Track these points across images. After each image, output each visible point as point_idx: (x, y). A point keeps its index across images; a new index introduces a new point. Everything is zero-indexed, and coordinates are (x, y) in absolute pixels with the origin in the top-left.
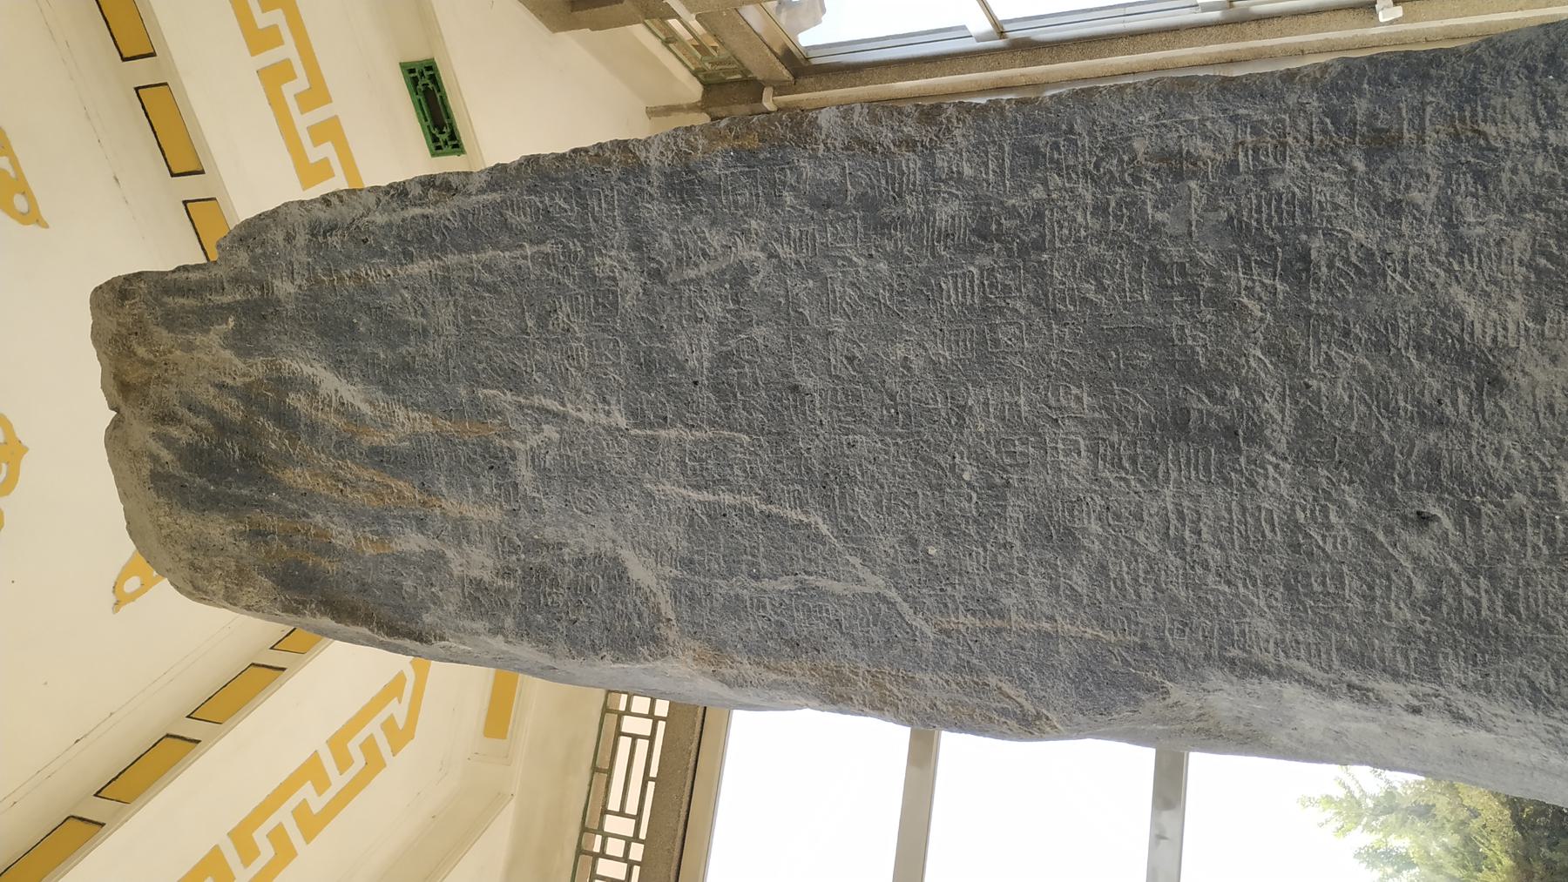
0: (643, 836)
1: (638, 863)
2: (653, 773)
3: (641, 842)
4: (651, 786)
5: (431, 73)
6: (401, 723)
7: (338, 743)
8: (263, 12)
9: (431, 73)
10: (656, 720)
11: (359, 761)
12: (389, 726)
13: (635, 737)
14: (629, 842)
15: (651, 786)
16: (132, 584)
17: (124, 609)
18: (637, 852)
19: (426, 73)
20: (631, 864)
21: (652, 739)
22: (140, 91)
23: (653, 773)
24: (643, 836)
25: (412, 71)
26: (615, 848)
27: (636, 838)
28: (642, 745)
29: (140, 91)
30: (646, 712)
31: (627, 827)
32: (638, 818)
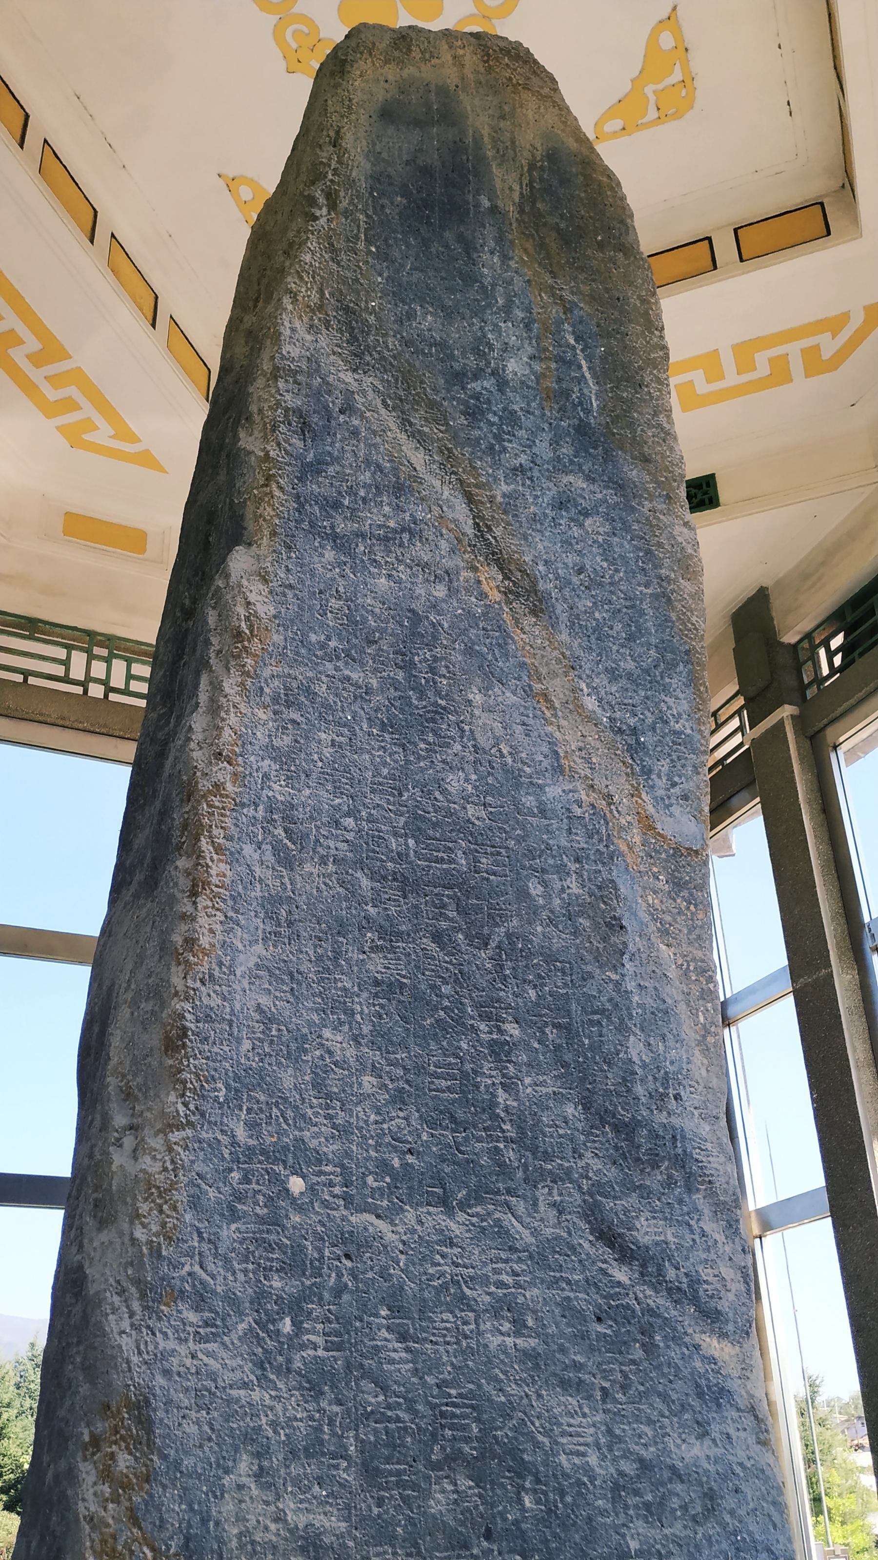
0: (113, 697)
1: (86, 692)
2: (32, 680)
3: (106, 696)
4: (19, 678)
5: (707, 501)
6: (826, 355)
7: (78, 377)
8: (802, 350)
9: (707, 501)
10: (84, 684)
11: (72, 391)
12: (89, 425)
13: (66, 663)
14: (105, 683)
15: (19, 678)
16: (246, 193)
17: (221, 182)
18: (96, 691)
19: (706, 497)
20: (84, 684)
21: (66, 679)
22: (707, 242)
23: (32, 680)
24: (113, 697)
25: (708, 485)
26: (98, 669)
27: (109, 690)
28: (60, 671)
29: (707, 242)
30: (93, 674)
31: (118, 681)
32: (126, 692)
